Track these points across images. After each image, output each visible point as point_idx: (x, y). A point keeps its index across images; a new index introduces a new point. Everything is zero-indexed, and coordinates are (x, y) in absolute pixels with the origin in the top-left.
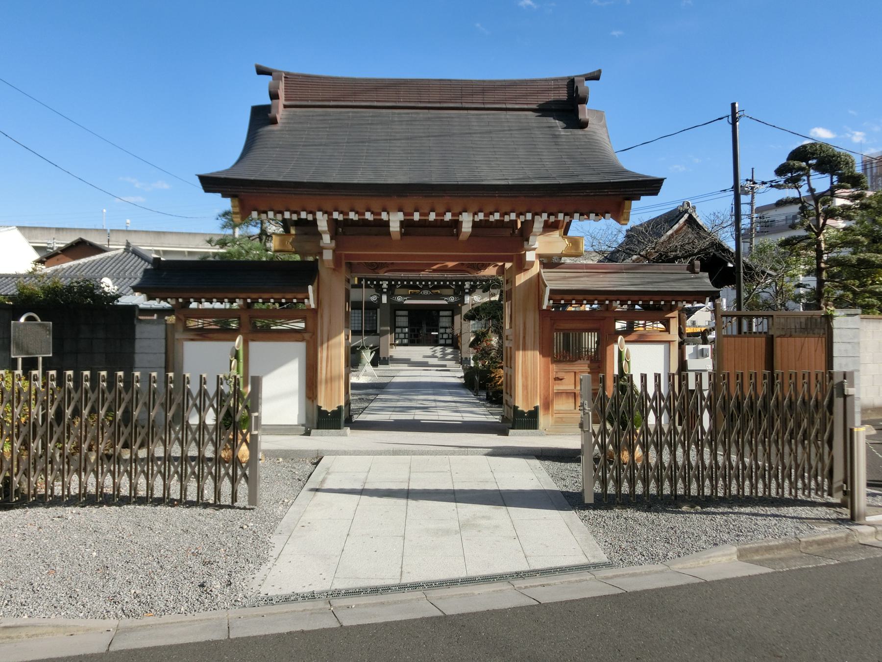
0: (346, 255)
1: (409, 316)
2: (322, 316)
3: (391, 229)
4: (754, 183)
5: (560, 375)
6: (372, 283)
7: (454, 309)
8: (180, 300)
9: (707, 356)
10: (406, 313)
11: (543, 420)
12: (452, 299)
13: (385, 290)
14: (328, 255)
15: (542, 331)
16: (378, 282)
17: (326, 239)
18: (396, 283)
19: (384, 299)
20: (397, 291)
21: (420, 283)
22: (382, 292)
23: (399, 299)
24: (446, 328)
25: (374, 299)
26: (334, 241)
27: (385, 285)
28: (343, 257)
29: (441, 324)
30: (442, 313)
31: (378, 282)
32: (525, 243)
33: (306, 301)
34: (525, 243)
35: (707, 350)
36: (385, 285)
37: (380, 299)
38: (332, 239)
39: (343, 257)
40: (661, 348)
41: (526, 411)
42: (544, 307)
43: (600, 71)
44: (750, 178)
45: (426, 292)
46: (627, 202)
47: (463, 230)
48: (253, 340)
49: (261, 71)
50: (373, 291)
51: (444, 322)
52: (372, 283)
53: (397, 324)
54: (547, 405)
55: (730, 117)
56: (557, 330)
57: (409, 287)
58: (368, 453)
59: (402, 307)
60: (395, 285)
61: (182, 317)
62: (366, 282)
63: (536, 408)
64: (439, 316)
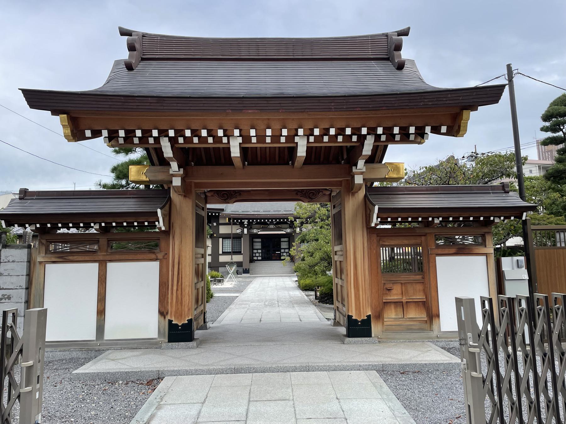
0: (195, 183)
1: (262, 242)
2: (173, 237)
3: (232, 155)
4: (477, 154)
5: (388, 286)
6: (237, 221)
7: (290, 237)
8: (38, 226)
9: (522, 267)
10: (260, 240)
11: (375, 328)
12: (289, 231)
13: (246, 226)
14: (177, 182)
15: (370, 249)
16: (241, 221)
17: (174, 165)
18: (253, 221)
19: (246, 231)
20: (253, 226)
21: (268, 221)
22: (244, 227)
23: (255, 231)
24: (285, 249)
25: (239, 231)
26: (182, 170)
27: (246, 222)
28: (193, 185)
29: (282, 247)
30: (282, 240)
31: (241, 221)
32: (354, 168)
33: (157, 223)
34: (354, 168)
35: (522, 261)
36: (246, 222)
37: (243, 231)
38: (179, 167)
39: (193, 185)
40: (484, 258)
41: (359, 320)
42: (373, 225)
43: (409, 28)
44: (474, 151)
45: (272, 226)
46: (465, 112)
47: (299, 154)
48: (111, 261)
49: (124, 32)
50: (238, 227)
51: (284, 245)
52: (237, 221)
53: (255, 247)
54: (379, 316)
55: (506, 76)
56: (383, 246)
57: (260, 223)
58: (209, 372)
59: (257, 236)
60: (252, 222)
61: (44, 241)
62: (233, 221)
63: (369, 317)
64: (281, 242)
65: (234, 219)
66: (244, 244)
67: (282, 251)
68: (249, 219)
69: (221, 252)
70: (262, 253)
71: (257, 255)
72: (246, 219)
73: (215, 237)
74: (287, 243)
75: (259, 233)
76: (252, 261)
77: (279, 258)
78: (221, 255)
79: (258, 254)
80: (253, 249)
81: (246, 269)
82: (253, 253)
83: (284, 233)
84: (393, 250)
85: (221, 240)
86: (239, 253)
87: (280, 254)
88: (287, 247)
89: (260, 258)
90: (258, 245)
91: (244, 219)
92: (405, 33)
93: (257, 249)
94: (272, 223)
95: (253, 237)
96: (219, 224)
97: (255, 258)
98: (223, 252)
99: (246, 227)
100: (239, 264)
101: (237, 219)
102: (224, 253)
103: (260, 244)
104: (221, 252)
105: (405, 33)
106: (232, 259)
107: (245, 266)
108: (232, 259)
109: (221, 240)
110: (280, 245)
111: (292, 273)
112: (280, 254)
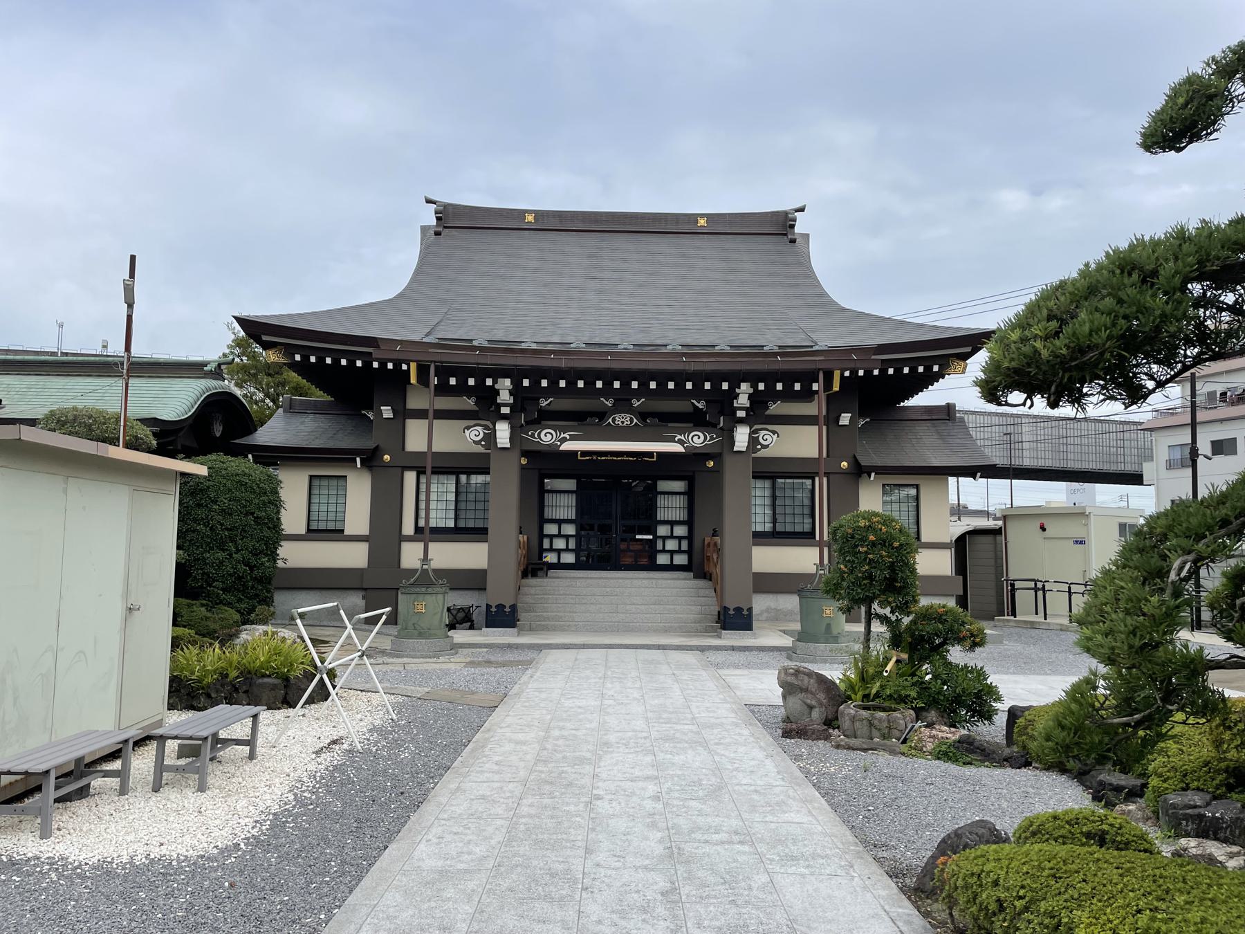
1: (579, 492)
10: (570, 484)
12: (698, 439)
13: (505, 410)
19: (503, 432)
23: (547, 437)
24: (672, 523)
29: (662, 515)
30: (663, 485)
37: (490, 438)
45: (623, 419)
51: (671, 507)
53: (550, 513)
65: (444, 371)
66: (503, 492)
67: (662, 530)
68: (515, 374)
69: (408, 528)
70: (577, 536)
71: (560, 544)
72: (505, 373)
73: (387, 466)
74: (680, 501)
75: (568, 446)
76: (534, 567)
77: (646, 561)
78: (409, 539)
79: (562, 541)
80: (543, 521)
81: (501, 607)
82: (542, 536)
83: (678, 448)
84: (547, 550)
85: (410, 477)
86: (478, 533)
87: (652, 543)
88: (680, 515)
89: (569, 558)
90: (563, 506)
91: (499, 373)
92: (802, 210)
93: (560, 522)
94: (622, 402)
95: (543, 466)
96: (403, 413)
97: (551, 558)
98: (418, 530)
99: (504, 417)
100: (472, 580)
101: (463, 372)
102: (425, 534)
103: (571, 500)
104: (408, 528)
105: (802, 210)
106: (426, 559)
107: (498, 594)
108: (426, 559)
109: (410, 477)
110: (652, 508)
111: (707, 631)
112: (652, 543)
